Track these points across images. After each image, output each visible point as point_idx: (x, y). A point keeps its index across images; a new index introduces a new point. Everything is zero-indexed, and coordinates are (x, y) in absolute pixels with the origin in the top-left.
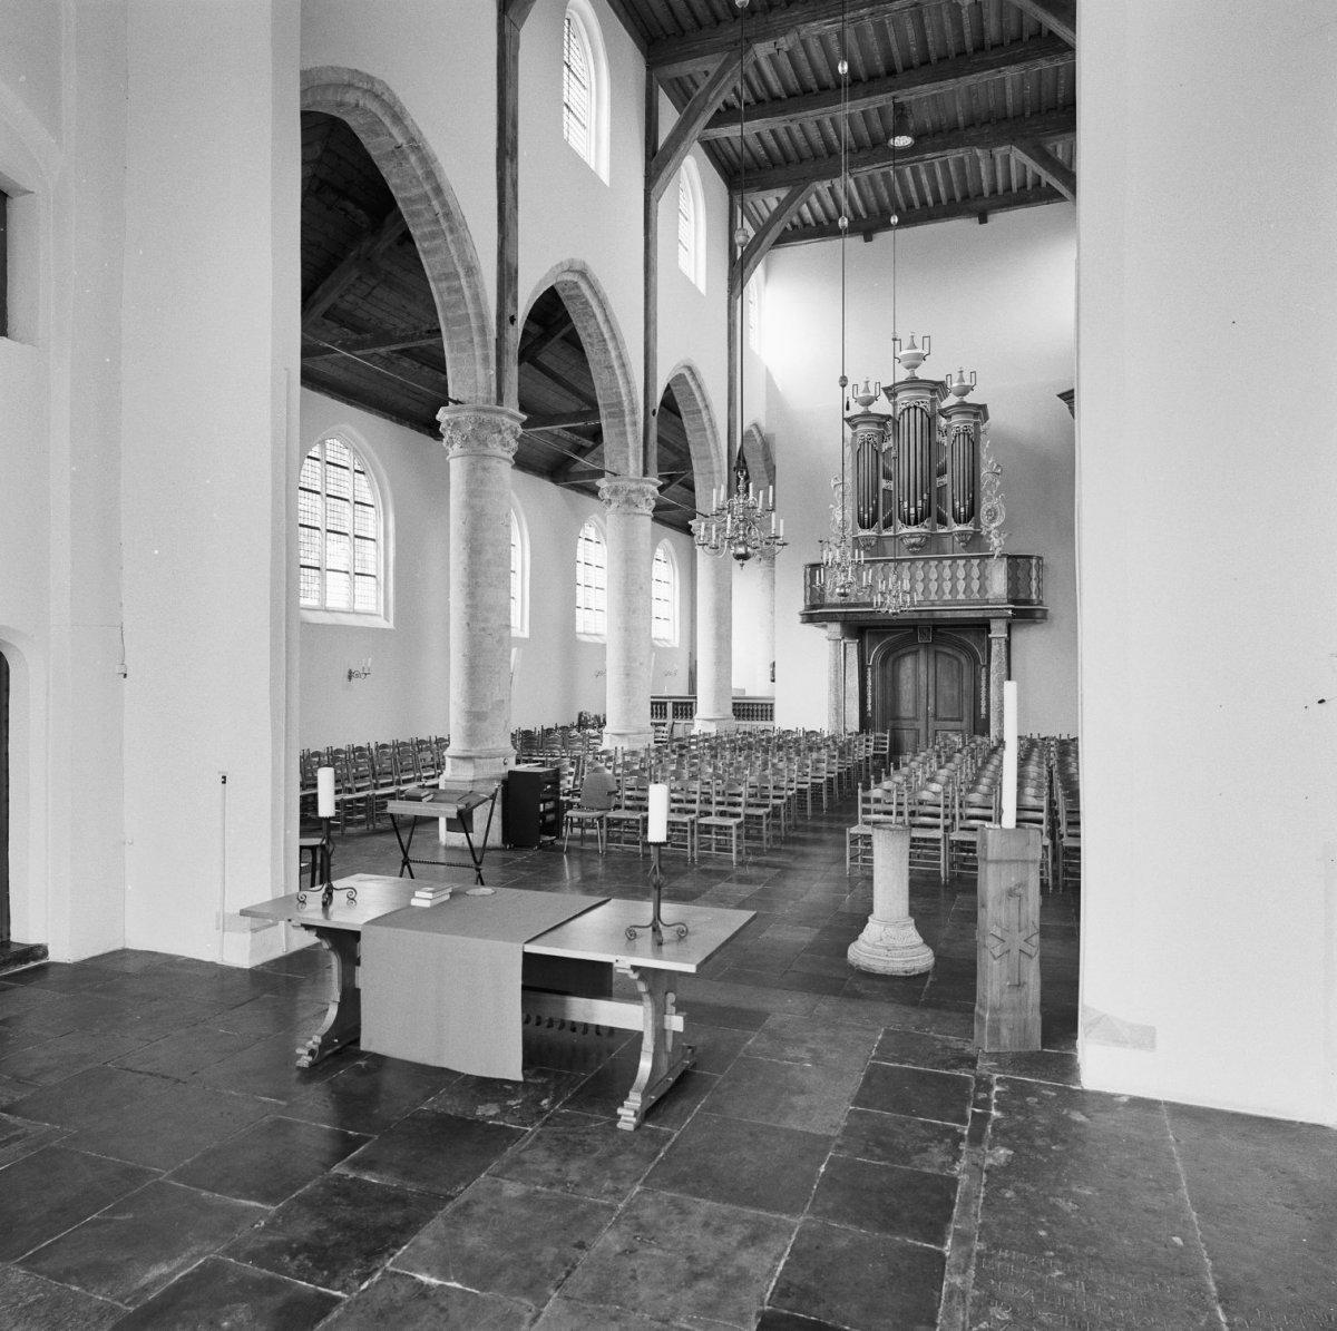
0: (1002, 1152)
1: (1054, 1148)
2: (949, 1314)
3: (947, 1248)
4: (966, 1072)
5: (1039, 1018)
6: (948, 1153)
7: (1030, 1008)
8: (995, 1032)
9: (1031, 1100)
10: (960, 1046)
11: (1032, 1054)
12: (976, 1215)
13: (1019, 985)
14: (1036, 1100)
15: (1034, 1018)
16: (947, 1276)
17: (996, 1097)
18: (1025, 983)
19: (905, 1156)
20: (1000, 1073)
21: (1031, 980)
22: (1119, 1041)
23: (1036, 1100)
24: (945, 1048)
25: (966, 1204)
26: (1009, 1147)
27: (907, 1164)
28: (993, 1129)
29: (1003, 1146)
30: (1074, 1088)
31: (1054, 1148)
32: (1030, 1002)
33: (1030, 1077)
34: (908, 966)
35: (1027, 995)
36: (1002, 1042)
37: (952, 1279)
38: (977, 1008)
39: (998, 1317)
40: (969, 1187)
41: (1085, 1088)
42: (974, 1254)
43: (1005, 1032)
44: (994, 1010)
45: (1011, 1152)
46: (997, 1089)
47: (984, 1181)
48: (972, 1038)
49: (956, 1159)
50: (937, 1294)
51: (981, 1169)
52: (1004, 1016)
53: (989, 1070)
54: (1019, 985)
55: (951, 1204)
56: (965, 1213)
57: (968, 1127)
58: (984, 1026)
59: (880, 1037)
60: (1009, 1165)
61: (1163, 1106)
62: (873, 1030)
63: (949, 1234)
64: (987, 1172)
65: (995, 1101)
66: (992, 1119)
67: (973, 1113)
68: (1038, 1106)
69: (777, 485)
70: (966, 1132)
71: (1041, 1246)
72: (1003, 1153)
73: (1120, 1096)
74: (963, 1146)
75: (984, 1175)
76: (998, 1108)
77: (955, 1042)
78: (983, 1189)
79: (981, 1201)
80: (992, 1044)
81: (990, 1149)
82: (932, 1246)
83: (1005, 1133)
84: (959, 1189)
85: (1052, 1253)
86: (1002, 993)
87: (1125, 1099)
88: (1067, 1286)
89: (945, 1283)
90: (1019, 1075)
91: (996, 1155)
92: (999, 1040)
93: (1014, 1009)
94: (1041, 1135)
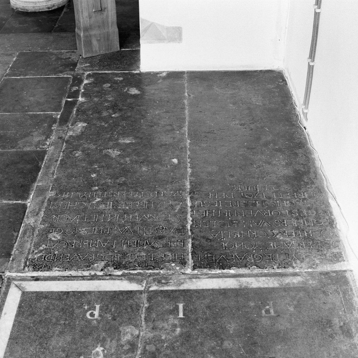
0: (80, 125)
1: (113, 116)
2: (21, 246)
3: (29, 201)
4: (67, 74)
5: (117, 30)
6: (44, 134)
7: (110, 24)
8: (88, 43)
9: (107, 85)
10: (68, 55)
11: (113, 54)
12: (53, 174)
13: (102, 10)
14: (109, 85)
15: (114, 31)
16: (25, 219)
17: (84, 88)
18: (105, 8)
19: (13, 142)
20: (90, 70)
21: (109, 6)
22: (160, 39)
23: (109, 85)
24: (58, 59)
25: (48, 167)
26: (85, 121)
27: (13, 147)
28: (78, 111)
29: (81, 121)
30: (135, 72)
31: (113, 116)
32: (110, 20)
33: (108, 70)
34: (50, 4)
35: (107, 17)
36: (94, 50)
37: (29, 220)
38: (76, 30)
39: (53, 239)
40: (53, 154)
41: (142, 71)
42: (46, 201)
43: (95, 43)
44: (86, 30)
45: (85, 125)
46: (86, 82)
47: (64, 148)
48: (76, 49)
49: (48, 137)
50: (16, 234)
51: (64, 140)
52: (93, 33)
53: (84, 70)
54: (101, 10)
55: (39, 169)
56: (46, 174)
57: (60, 113)
58: (81, 41)
59: (14, 59)
60: (82, 133)
61: (185, 75)
62: (11, 55)
63: (32, 190)
64: (67, 142)
65: (83, 91)
66: (78, 103)
67: (67, 101)
68: (110, 89)
69: (314, 12)
70: (59, 117)
71: (91, 184)
72: (81, 125)
73: (161, 72)
74: (54, 127)
75: (65, 144)
76: (84, 95)
77: (65, 53)
78: (61, 154)
79: (59, 162)
80: (86, 52)
81: (72, 125)
82: (20, 202)
83: (84, 112)
84: (46, 158)
85: (97, 188)
86: (90, 18)
87: (164, 74)
88: (102, 207)
89: (23, 225)
90: (102, 70)
91: (75, 129)
92: (92, 49)
93: (99, 27)
94: (107, 108)
